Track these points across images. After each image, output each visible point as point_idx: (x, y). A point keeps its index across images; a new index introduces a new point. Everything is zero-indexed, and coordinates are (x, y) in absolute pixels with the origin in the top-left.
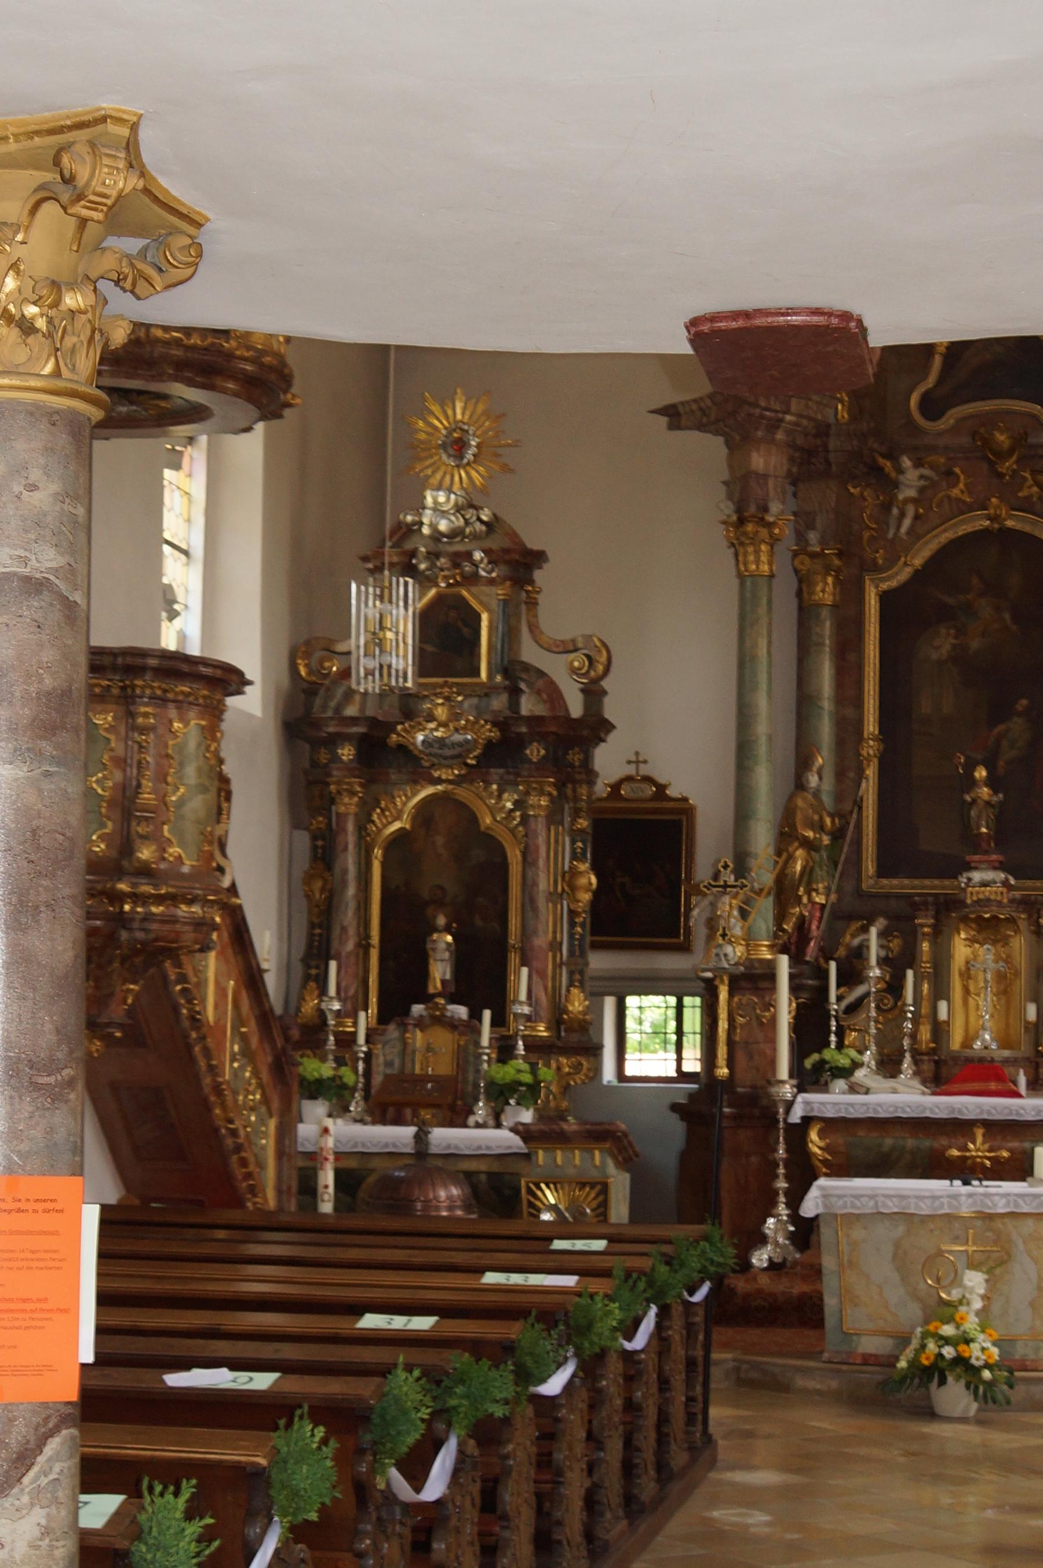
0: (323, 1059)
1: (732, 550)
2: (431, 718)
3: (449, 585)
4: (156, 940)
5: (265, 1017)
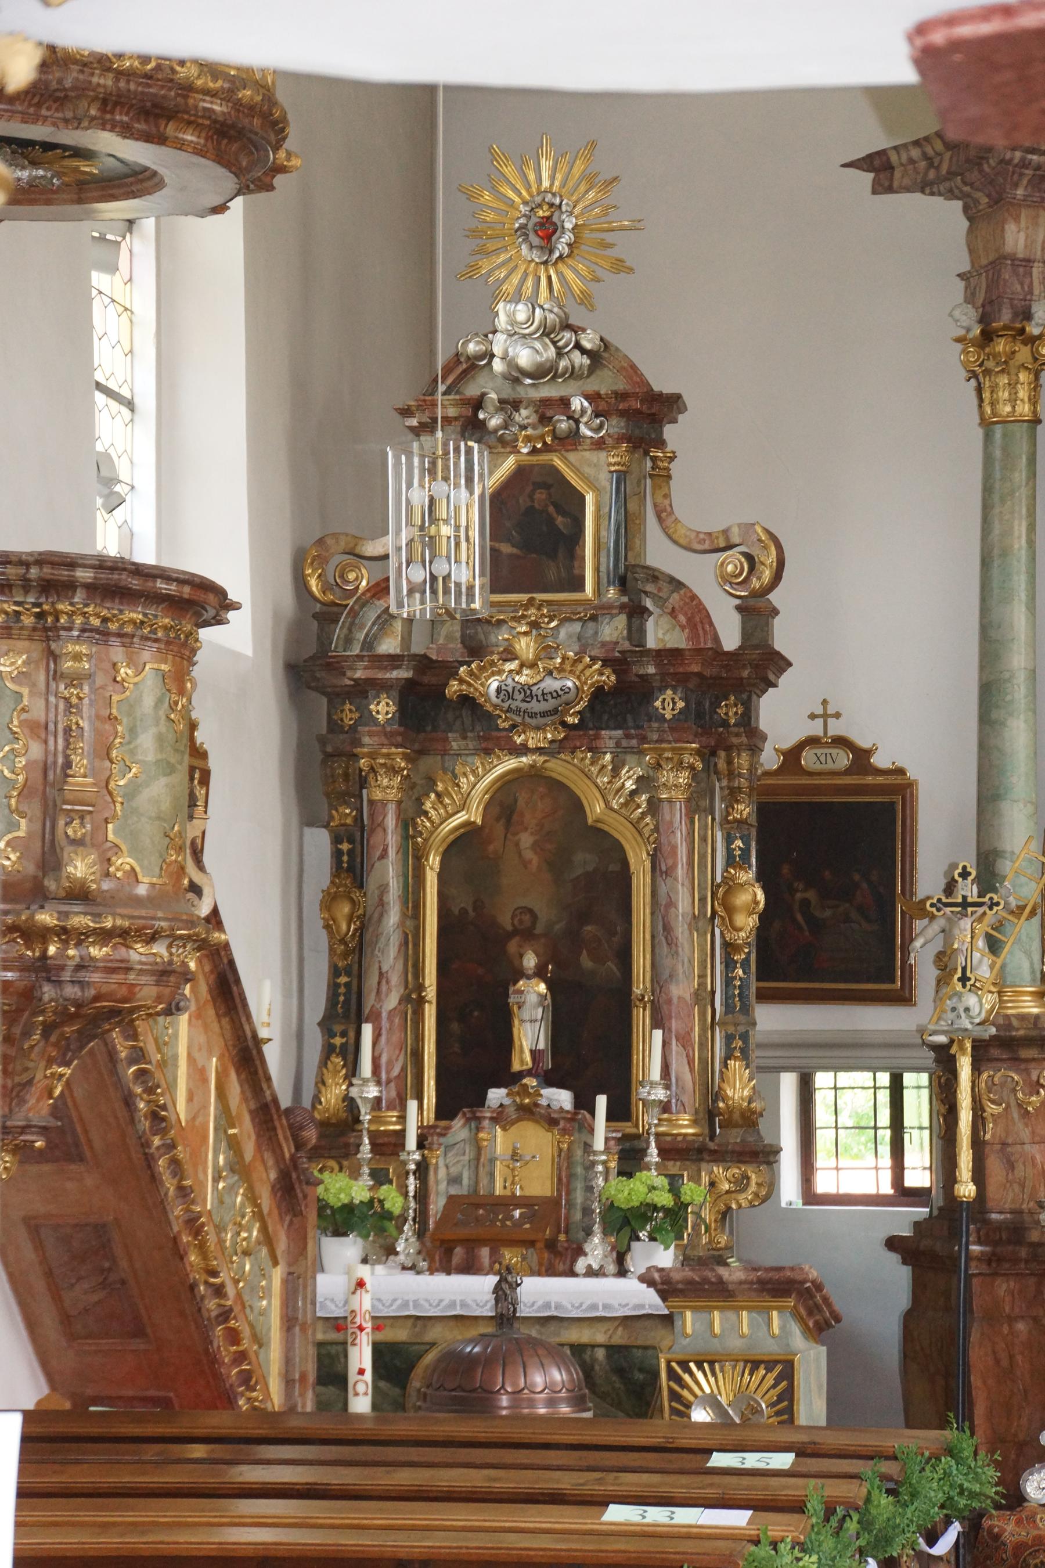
0: (355, 1175)
1: (973, 382)
2: (509, 654)
3: (534, 451)
4: (97, 998)
5: (265, 1112)
